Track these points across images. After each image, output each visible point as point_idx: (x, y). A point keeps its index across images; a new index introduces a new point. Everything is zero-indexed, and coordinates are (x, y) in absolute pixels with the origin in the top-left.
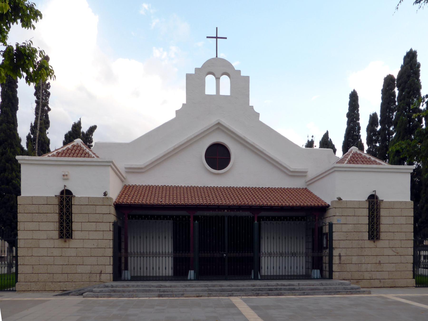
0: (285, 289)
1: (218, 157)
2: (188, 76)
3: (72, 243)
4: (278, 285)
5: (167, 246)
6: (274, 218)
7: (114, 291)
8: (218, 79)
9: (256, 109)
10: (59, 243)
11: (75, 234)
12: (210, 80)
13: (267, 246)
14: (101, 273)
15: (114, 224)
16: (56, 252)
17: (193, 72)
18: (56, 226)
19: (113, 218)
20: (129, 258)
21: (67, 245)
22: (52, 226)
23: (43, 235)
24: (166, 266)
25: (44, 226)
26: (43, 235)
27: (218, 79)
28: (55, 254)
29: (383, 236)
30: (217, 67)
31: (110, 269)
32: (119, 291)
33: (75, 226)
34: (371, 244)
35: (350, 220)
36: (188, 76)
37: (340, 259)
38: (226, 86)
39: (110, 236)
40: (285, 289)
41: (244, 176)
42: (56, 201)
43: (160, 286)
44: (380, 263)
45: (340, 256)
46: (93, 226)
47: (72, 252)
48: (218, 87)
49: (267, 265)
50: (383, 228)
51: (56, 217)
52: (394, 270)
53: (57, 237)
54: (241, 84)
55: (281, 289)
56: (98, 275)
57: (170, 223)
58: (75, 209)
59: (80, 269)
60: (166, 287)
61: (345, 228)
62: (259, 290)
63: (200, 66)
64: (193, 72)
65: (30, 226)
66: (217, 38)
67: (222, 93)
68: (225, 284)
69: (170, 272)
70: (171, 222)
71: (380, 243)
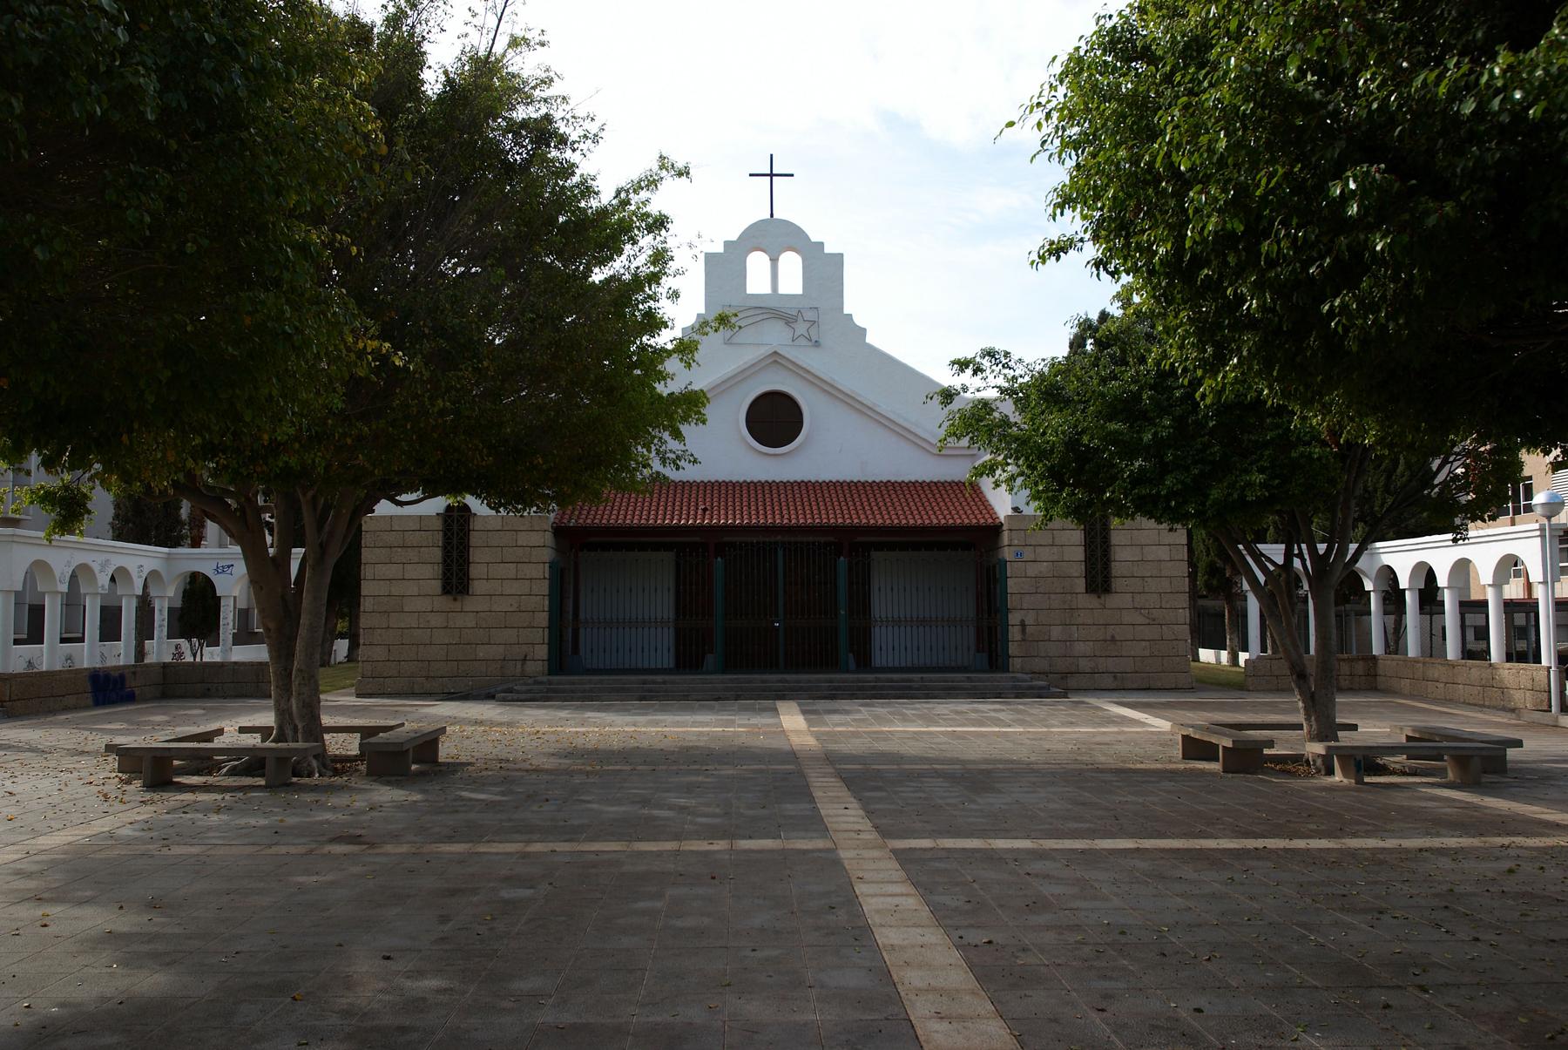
0: (892, 688)
1: (775, 419)
2: (710, 258)
3: (470, 604)
4: (877, 680)
5: (661, 603)
6: (891, 547)
7: (555, 691)
8: (774, 261)
9: (859, 321)
10: (445, 603)
11: (478, 587)
12: (757, 264)
13: (883, 603)
14: (525, 660)
15: (552, 565)
16: (436, 620)
17: (721, 249)
18: (438, 570)
19: (547, 555)
20: (582, 631)
21: (457, 606)
22: (426, 572)
23: (413, 589)
24: (660, 646)
25: (412, 571)
26: (413, 589)
27: (774, 261)
28: (433, 623)
29: (1117, 584)
30: (773, 235)
31: (542, 652)
32: (564, 691)
33: (475, 571)
34: (1091, 601)
35: (1045, 553)
36: (710, 258)
37: (1023, 631)
38: (791, 276)
39: (544, 587)
40: (892, 688)
41: (830, 452)
42: (438, 525)
43: (644, 683)
44: (1113, 640)
45: (1023, 625)
46: (510, 570)
47: (470, 621)
48: (774, 277)
49: (886, 644)
50: (1117, 569)
51: (437, 554)
52: (1147, 653)
53: (439, 590)
54: (825, 270)
55: (882, 688)
56: (519, 664)
57: (669, 557)
58: (475, 539)
59: (482, 652)
60: (654, 682)
61: (1032, 570)
62: (836, 689)
63: (735, 238)
64: (721, 249)
65: (383, 571)
66: (771, 175)
67: (783, 289)
68: (773, 678)
69: (668, 660)
70: (669, 557)
71: (1113, 601)
